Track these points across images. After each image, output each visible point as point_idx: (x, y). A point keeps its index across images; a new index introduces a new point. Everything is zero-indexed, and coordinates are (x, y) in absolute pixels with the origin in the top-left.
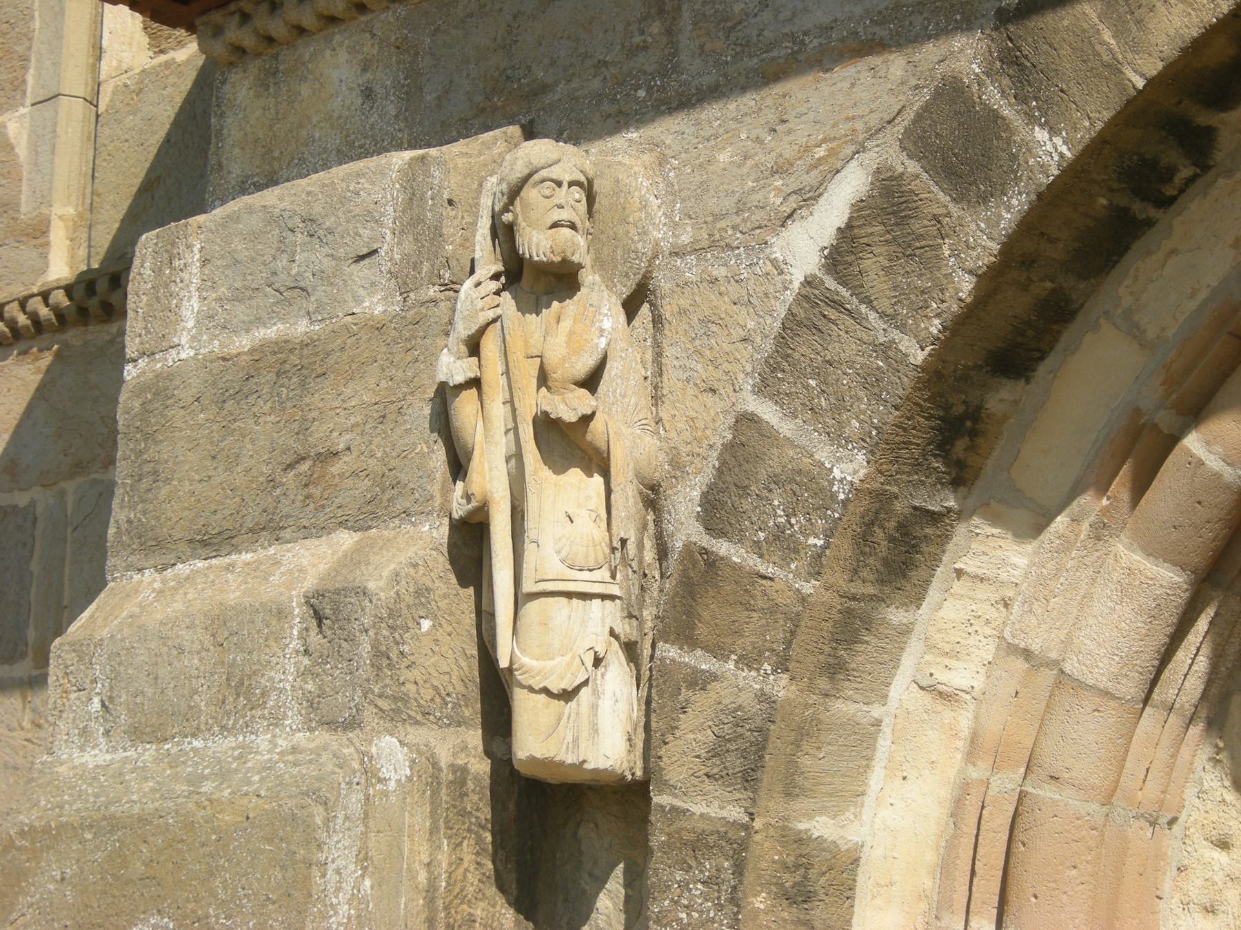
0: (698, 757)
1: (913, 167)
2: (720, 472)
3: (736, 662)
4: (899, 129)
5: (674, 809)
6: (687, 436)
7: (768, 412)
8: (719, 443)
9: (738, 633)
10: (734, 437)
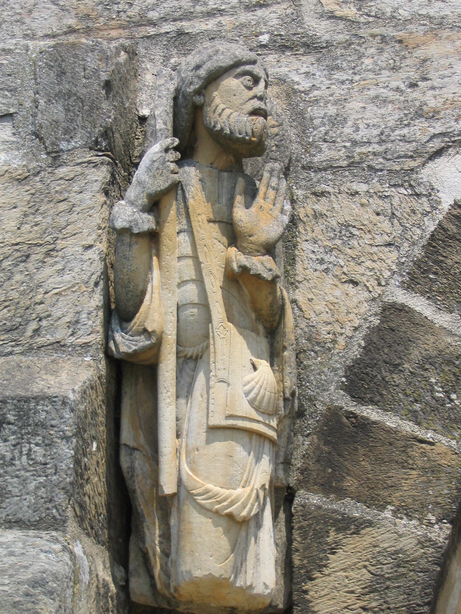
0: (352, 592)
3: (394, 512)
6: (325, 317)
7: (419, 304)
10: (382, 322)
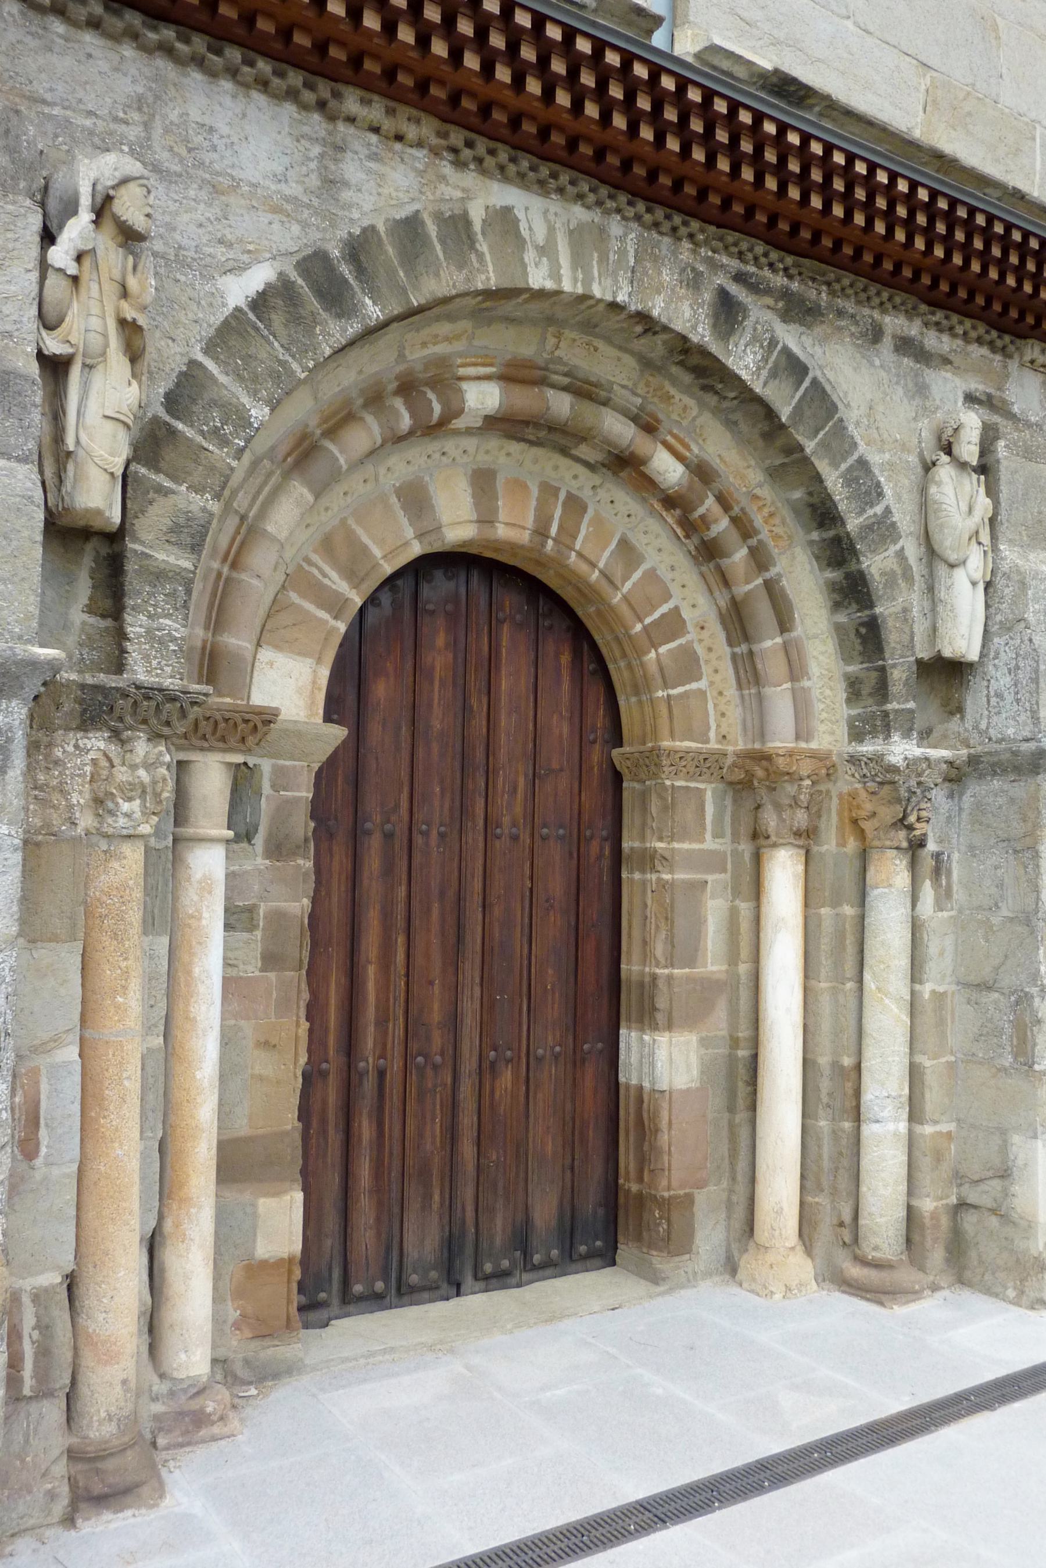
1: (300, 281)
2: (178, 385)
4: (294, 260)
5: (143, 553)
7: (210, 365)
8: (177, 370)
9: (190, 474)
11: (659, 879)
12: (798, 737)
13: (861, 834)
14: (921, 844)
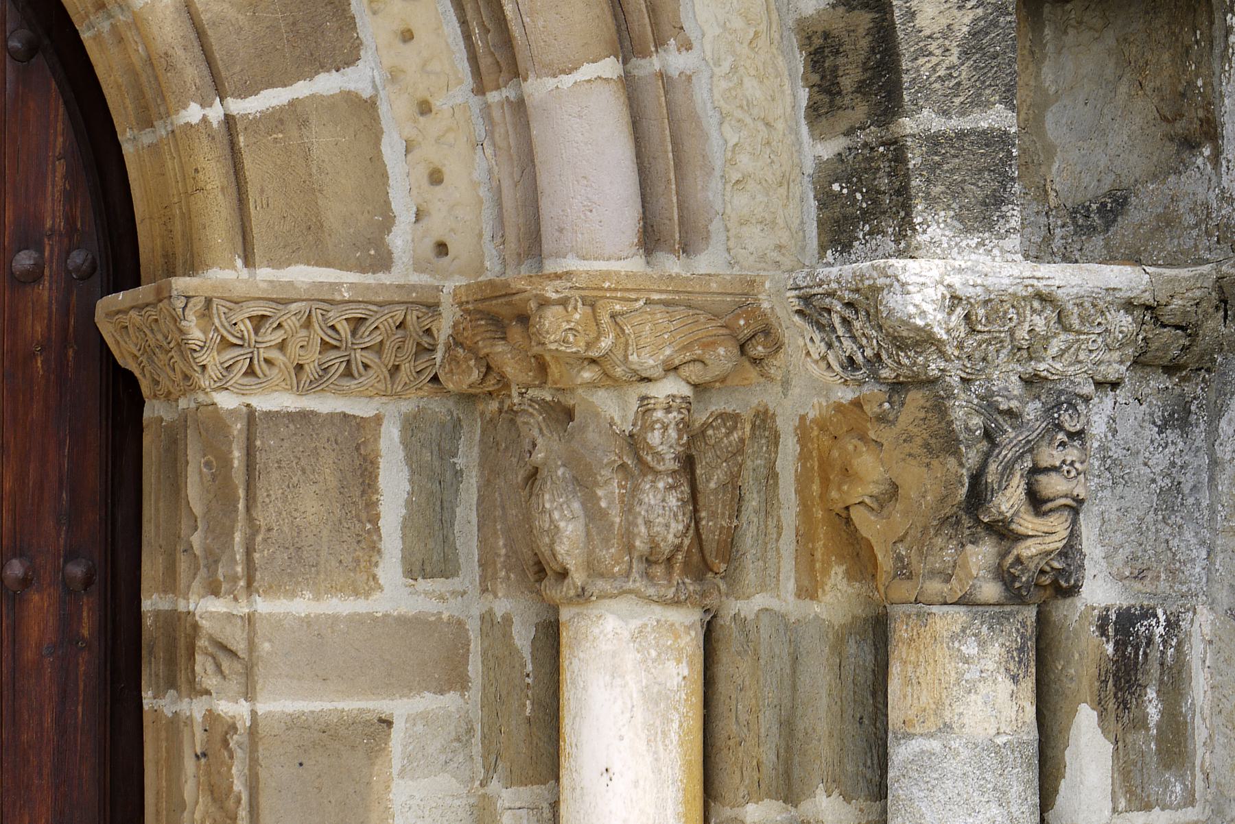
11: (212, 717)
12: (650, 239)
13: (859, 557)
14: (1060, 583)
